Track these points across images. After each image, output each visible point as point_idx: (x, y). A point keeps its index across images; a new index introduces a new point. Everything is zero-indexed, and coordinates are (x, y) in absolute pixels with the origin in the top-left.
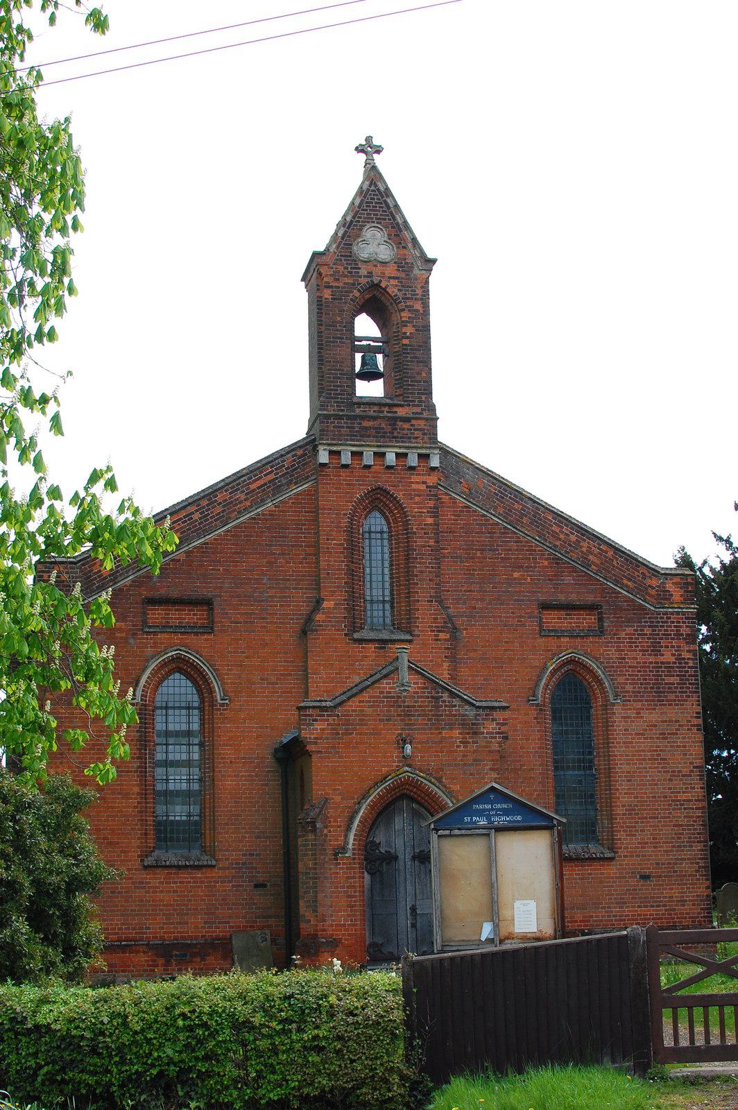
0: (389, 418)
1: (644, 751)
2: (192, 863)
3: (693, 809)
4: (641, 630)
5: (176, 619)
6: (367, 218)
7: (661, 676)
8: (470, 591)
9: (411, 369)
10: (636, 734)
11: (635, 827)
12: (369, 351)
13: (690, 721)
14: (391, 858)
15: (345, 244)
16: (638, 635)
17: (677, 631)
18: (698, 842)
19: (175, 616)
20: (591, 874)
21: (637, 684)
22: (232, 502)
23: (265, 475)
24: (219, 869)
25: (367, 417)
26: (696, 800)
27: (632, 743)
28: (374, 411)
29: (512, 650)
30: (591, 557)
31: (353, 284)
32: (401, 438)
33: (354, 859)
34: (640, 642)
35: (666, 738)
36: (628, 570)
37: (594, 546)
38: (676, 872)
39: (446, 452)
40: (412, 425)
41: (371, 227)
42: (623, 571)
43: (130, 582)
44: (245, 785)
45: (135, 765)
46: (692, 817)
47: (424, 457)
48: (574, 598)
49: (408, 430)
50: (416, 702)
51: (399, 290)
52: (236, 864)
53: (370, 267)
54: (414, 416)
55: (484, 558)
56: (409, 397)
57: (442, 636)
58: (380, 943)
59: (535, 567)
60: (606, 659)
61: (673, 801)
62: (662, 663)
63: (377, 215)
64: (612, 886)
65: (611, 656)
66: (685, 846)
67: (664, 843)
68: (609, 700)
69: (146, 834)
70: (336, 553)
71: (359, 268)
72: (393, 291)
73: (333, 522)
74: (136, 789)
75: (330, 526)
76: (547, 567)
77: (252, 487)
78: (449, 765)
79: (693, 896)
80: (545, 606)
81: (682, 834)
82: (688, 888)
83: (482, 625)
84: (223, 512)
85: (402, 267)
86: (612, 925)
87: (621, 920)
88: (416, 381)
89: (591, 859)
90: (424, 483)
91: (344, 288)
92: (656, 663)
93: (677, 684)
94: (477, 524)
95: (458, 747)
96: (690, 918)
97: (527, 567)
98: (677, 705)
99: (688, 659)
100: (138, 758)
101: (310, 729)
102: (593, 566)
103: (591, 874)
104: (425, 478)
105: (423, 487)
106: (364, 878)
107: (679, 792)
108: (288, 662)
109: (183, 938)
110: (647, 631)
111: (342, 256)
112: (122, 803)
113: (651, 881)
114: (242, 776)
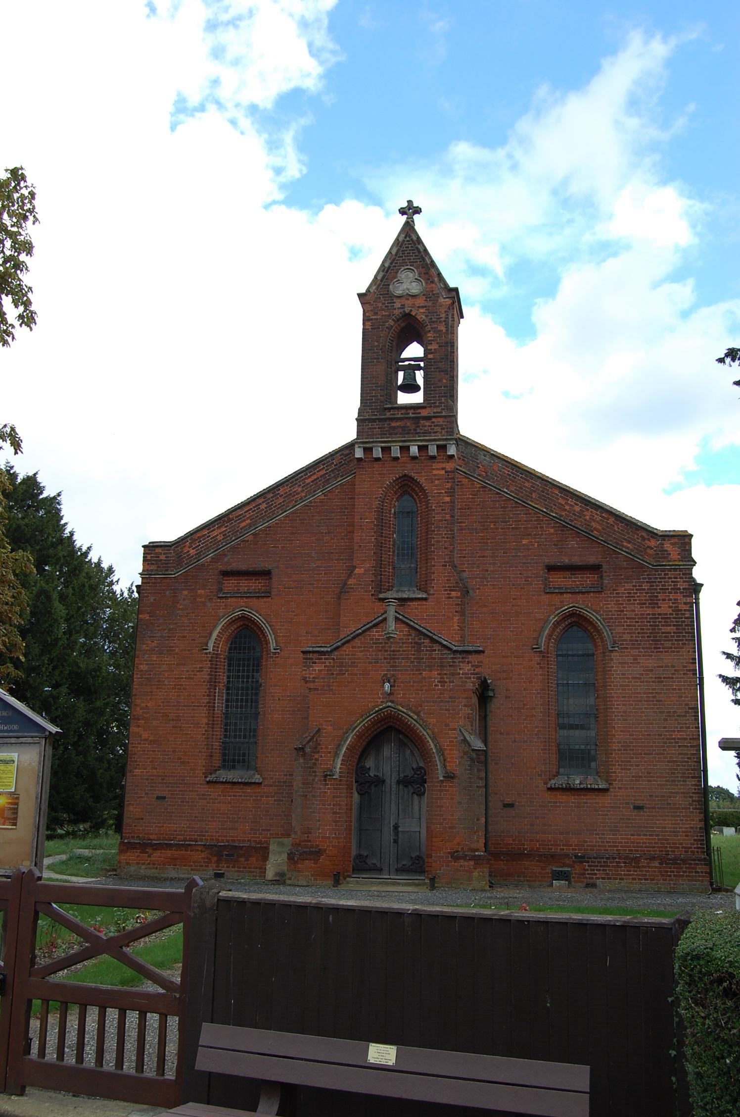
0: (413, 418)
1: (640, 693)
2: (243, 780)
3: (688, 746)
4: (639, 586)
5: (245, 586)
6: (402, 263)
7: (658, 626)
8: (484, 557)
9: (434, 378)
10: (633, 678)
11: (630, 762)
12: (410, 370)
13: (686, 667)
14: (379, 782)
15: (384, 285)
16: (636, 590)
17: (674, 585)
18: (692, 777)
19: (244, 585)
20: (586, 803)
21: (635, 633)
22: (291, 494)
23: (318, 472)
24: (265, 786)
25: (395, 418)
26: (690, 739)
27: (628, 686)
28: (401, 414)
29: (519, 606)
30: (593, 524)
31: (389, 316)
32: (423, 433)
33: (340, 781)
34: (638, 597)
35: (662, 682)
36: (629, 534)
37: (597, 514)
38: (668, 804)
39: (466, 444)
40: (432, 422)
41: (405, 269)
42: (623, 535)
43: (210, 559)
44: (289, 718)
45: (205, 701)
46: (687, 754)
47: (442, 448)
48: (576, 560)
49: (429, 426)
50: (400, 647)
51: (426, 316)
52: (278, 782)
53: (403, 301)
54: (434, 415)
55: (497, 529)
56: (431, 400)
57: (454, 594)
58: (366, 855)
59: (542, 534)
60: (606, 612)
61: (668, 739)
62: (659, 614)
63: (410, 259)
64: (607, 815)
65: (610, 609)
66: (679, 781)
67: (658, 777)
68: (608, 648)
69: (211, 756)
70: (367, 529)
71: (394, 303)
72: (421, 317)
73: (366, 505)
74: (205, 720)
75: (364, 508)
76: (552, 534)
77: (307, 481)
78: (427, 702)
79: (687, 828)
80: (551, 568)
81: (676, 769)
82: (682, 820)
83: (493, 585)
84: (283, 502)
85: (430, 297)
86: (605, 850)
87: (615, 846)
88: (439, 387)
89: (586, 790)
90: (443, 469)
91: (382, 319)
92: (653, 614)
93: (674, 633)
94: (492, 501)
95: (436, 685)
96: (682, 848)
97: (535, 535)
98: (674, 652)
99: (685, 610)
100: (208, 696)
101: (310, 670)
102: (595, 532)
103: (586, 803)
104: (444, 465)
105: (443, 472)
106: (352, 797)
107: (674, 731)
108: (328, 618)
109: (233, 841)
110: (646, 586)
111: (380, 295)
112: (193, 731)
113: (644, 812)
114: (287, 711)
